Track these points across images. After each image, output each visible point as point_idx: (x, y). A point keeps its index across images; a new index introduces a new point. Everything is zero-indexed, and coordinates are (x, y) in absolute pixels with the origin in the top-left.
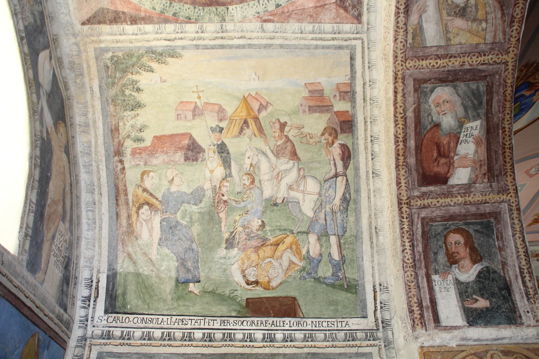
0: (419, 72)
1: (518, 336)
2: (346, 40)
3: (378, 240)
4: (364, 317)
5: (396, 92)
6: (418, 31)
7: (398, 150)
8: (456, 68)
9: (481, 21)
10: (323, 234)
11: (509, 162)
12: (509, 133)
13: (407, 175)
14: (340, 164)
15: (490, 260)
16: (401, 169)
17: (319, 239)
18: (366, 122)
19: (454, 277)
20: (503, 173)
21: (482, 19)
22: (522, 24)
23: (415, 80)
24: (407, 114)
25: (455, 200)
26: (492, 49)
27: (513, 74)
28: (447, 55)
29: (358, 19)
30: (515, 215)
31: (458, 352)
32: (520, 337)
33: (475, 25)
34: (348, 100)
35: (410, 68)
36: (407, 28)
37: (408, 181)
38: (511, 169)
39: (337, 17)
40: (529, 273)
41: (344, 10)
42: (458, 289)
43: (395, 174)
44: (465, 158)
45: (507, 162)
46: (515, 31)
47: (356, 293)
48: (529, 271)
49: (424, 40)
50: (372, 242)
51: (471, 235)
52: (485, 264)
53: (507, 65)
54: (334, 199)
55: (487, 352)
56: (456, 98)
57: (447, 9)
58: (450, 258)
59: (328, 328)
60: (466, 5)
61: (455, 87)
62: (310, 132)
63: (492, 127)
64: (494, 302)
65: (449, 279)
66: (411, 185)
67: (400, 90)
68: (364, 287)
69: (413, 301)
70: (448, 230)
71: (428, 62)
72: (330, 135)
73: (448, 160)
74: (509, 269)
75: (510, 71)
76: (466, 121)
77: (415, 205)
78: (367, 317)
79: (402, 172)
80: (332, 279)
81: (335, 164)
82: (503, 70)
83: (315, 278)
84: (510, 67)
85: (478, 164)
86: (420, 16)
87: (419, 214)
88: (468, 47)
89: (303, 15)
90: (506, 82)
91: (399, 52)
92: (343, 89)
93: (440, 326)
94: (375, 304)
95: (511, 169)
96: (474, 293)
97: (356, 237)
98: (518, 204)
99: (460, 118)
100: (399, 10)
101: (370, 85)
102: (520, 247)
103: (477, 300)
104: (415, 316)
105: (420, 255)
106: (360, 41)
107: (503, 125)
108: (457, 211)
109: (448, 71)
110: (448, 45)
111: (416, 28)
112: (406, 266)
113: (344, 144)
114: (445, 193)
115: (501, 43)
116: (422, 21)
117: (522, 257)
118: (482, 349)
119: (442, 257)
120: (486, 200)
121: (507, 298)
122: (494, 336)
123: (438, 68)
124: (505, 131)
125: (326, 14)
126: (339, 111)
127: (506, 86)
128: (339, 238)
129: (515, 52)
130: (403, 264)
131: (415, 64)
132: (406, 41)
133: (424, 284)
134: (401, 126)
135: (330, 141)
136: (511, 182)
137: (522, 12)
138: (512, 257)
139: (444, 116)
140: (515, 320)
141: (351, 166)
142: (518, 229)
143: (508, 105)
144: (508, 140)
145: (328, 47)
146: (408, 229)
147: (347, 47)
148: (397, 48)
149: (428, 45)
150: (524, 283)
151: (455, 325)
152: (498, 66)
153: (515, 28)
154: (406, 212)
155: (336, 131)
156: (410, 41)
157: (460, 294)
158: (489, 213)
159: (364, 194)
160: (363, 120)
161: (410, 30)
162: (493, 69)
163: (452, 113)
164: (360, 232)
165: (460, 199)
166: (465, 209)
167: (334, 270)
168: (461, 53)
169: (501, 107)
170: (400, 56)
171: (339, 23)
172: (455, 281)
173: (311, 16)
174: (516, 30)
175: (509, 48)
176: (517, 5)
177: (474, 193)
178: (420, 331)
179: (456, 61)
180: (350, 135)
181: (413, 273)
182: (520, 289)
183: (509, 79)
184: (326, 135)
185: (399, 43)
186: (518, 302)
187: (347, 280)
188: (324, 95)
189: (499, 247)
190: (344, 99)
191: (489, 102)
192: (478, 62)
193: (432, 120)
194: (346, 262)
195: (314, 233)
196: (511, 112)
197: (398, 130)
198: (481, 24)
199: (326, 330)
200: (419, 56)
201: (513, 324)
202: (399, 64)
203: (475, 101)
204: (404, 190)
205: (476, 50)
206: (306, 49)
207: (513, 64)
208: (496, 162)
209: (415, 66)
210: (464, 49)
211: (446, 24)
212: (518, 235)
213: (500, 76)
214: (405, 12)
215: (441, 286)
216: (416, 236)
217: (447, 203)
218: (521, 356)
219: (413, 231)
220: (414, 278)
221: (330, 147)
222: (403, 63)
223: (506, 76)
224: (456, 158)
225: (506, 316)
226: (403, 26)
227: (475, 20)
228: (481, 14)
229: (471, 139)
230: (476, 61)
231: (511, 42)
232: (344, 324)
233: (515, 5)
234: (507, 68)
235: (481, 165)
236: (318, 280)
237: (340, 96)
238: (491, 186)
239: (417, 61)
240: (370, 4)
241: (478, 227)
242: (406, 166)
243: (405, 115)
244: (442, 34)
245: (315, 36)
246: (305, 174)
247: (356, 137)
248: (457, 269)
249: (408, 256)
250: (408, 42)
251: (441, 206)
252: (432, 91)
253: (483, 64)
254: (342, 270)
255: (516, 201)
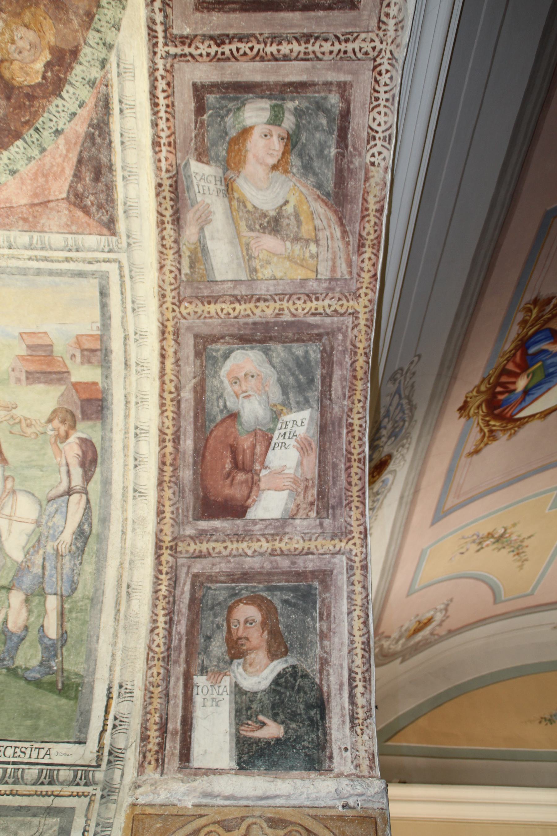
0: (204, 323)
1: (302, 793)
2: (90, 263)
3: (128, 606)
4: (80, 743)
5: (163, 356)
6: (200, 255)
7: (164, 456)
8: (268, 320)
9: (307, 241)
10: (36, 592)
11: (356, 485)
12: (360, 435)
13: (175, 500)
14: (77, 473)
15: (301, 654)
16: (166, 489)
17: (27, 600)
18: (127, 403)
19: (234, 680)
20: (345, 503)
21: (308, 237)
22: (378, 251)
23: (196, 336)
24: (182, 394)
25: (255, 546)
26: (331, 289)
27: (367, 333)
28: (252, 296)
29: (109, 229)
30: (358, 577)
31: (193, 818)
32: (305, 796)
33: (297, 247)
34: (96, 363)
35: (187, 316)
36: (179, 249)
37: (177, 509)
38: (359, 496)
39: (72, 223)
40: (365, 681)
41: (84, 212)
42: (236, 703)
43: (156, 496)
44: (279, 473)
45: (353, 483)
46: (367, 261)
47: (76, 698)
48: (365, 678)
49: (210, 269)
50: (119, 610)
51: (276, 609)
52: (291, 660)
53: (357, 318)
54: (62, 532)
55: (243, 819)
56: (268, 371)
57: (247, 220)
58: (233, 647)
59: (12, 760)
60: (278, 213)
61: (266, 352)
62: (28, 416)
63: (329, 422)
64: (293, 729)
65: (223, 684)
66: (181, 516)
67: (170, 351)
68: (92, 688)
69: (152, 721)
70: (237, 598)
71: (219, 306)
72: (63, 422)
73: (250, 475)
74: (331, 671)
75: (362, 327)
76: (285, 410)
77: (184, 551)
78: (85, 743)
79: (168, 493)
80: (39, 672)
81: (68, 472)
82: (350, 325)
83: (8, 669)
84: (362, 322)
85: (302, 486)
86: (202, 229)
87: (189, 567)
88: (288, 284)
89: (11, 218)
90: (355, 346)
91: (168, 288)
92: (87, 345)
93: (187, 767)
94: (106, 719)
95: (359, 496)
96: (262, 712)
97: (92, 600)
98: (366, 558)
99: (275, 405)
100: (164, 218)
101: (136, 340)
102: (357, 633)
103: (263, 724)
104: (150, 746)
105: (180, 640)
106: (116, 265)
107: (350, 421)
108: (257, 566)
109: (255, 324)
110: (253, 280)
111: (196, 248)
112: (153, 657)
113: (86, 440)
114: (240, 532)
115: (346, 279)
116: (204, 237)
117: (359, 652)
118: (237, 814)
119: (218, 644)
120: (309, 548)
121: (317, 723)
122: (259, 793)
123: (236, 317)
124: (353, 430)
125: (51, 217)
126: (80, 383)
127: (356, 353)
128: (63, 599)
129: (369, 297)
130: (148, 654)
131: (196, 310)
132: (180, 270)
133: (178, 691)
134: (171, 415)
135: (62, 432)
136: (357, 520)
137: (375, 231)
138: (340, 650)
139: (246, 401)
140: (320, 762)
141: (97, 476)
142: (359, 602)
143: (359, 385)
144: (357, 447)
145: (60, 273)
146: (166, 593)
147: (93, 274)
148: (164, 281)
149: (218, 278)
150: (352, 697)
151: (215, 767)
152: (342, 318)
153: (366, 256)
154: (168, 562)
155: (73, 416)
156: (186, 270)
157: (236, 711)
158: (312, 572)
159: (115, 527)
160: (123, 398)
161: (186, 253)
162: (332, 323)
163: (260, 395)
164: (100, 592)
165: (265, 546)
166: (271, 562)
167: (45, 655)
168: (276, 295)
169: (347, 389)
170: (170, 295)
171: (77, 233)
172: (233, 689)
173: (25, 220)
174: (370, 259)
175: (358, 289)
176: (367, 219)
177: (291, 536)
178: (152, 774)
179: (268, 307)
180: (99, 423)
181: (162, 671)
182: (343, 708)
183: (361, 341)
184: (56, 423)
185: (167, 273)
186: (333, 732)
187: (65, 674)
188: (54, 354)
189: (321, 631)
190: (89, 362)
191: (327, 380)
192: (306, 311)
193: (225, 406)
194: (68, 643)
195: (20, 589)
196: (366, 398)
197: (166, 420)
198: (307, 246)
199: (8, 763)
200: (203, 297)
201: (315, 769)
202: (167, 309)
203: (301, 377)
204: (168, 525)
205: (303, 290)
206: (19, 274)
207: (367, 316)
208: (334, 484)
209: (196, 313)
210: (281, 287)
211: (248, 244)
212: (357, 612)
213: (345, 336)
214: (173, 221)
215: (207, 697)
216: (179, 605)
217: (240, 551)
218: (300, 829)
219: (174, 597)
220: (163, 680)
221: (61, 443)
222: (176, 308)
223: (356, 337)
224: (263, 473)
225: (306, 755)
226: (173, 245)
227: (296, 239)
228: (306, 230)
229: (293, 442)
230: (303, 309)
231: (361, 280)
232: (43, 752)
233: (363, 218)
234: (356, 322)
235: (307, 487)
236: (13, 672)
237: (83, 356)
238: (321, 524)
239: (200, 305)
240: (129, 203)
241: (289, 596)
242: (176, 484)
243: (179, 395)
244: (242, 260)
245: (35, 253)
246: (15, 488)
247: (108, 427)
248: (241, 667)
249: (159, 640)
250: (183, 272)
251: (230, 555)
252: (226, 357)
253: (314, 314)
254: (59, 655)
255: (362, 553)
